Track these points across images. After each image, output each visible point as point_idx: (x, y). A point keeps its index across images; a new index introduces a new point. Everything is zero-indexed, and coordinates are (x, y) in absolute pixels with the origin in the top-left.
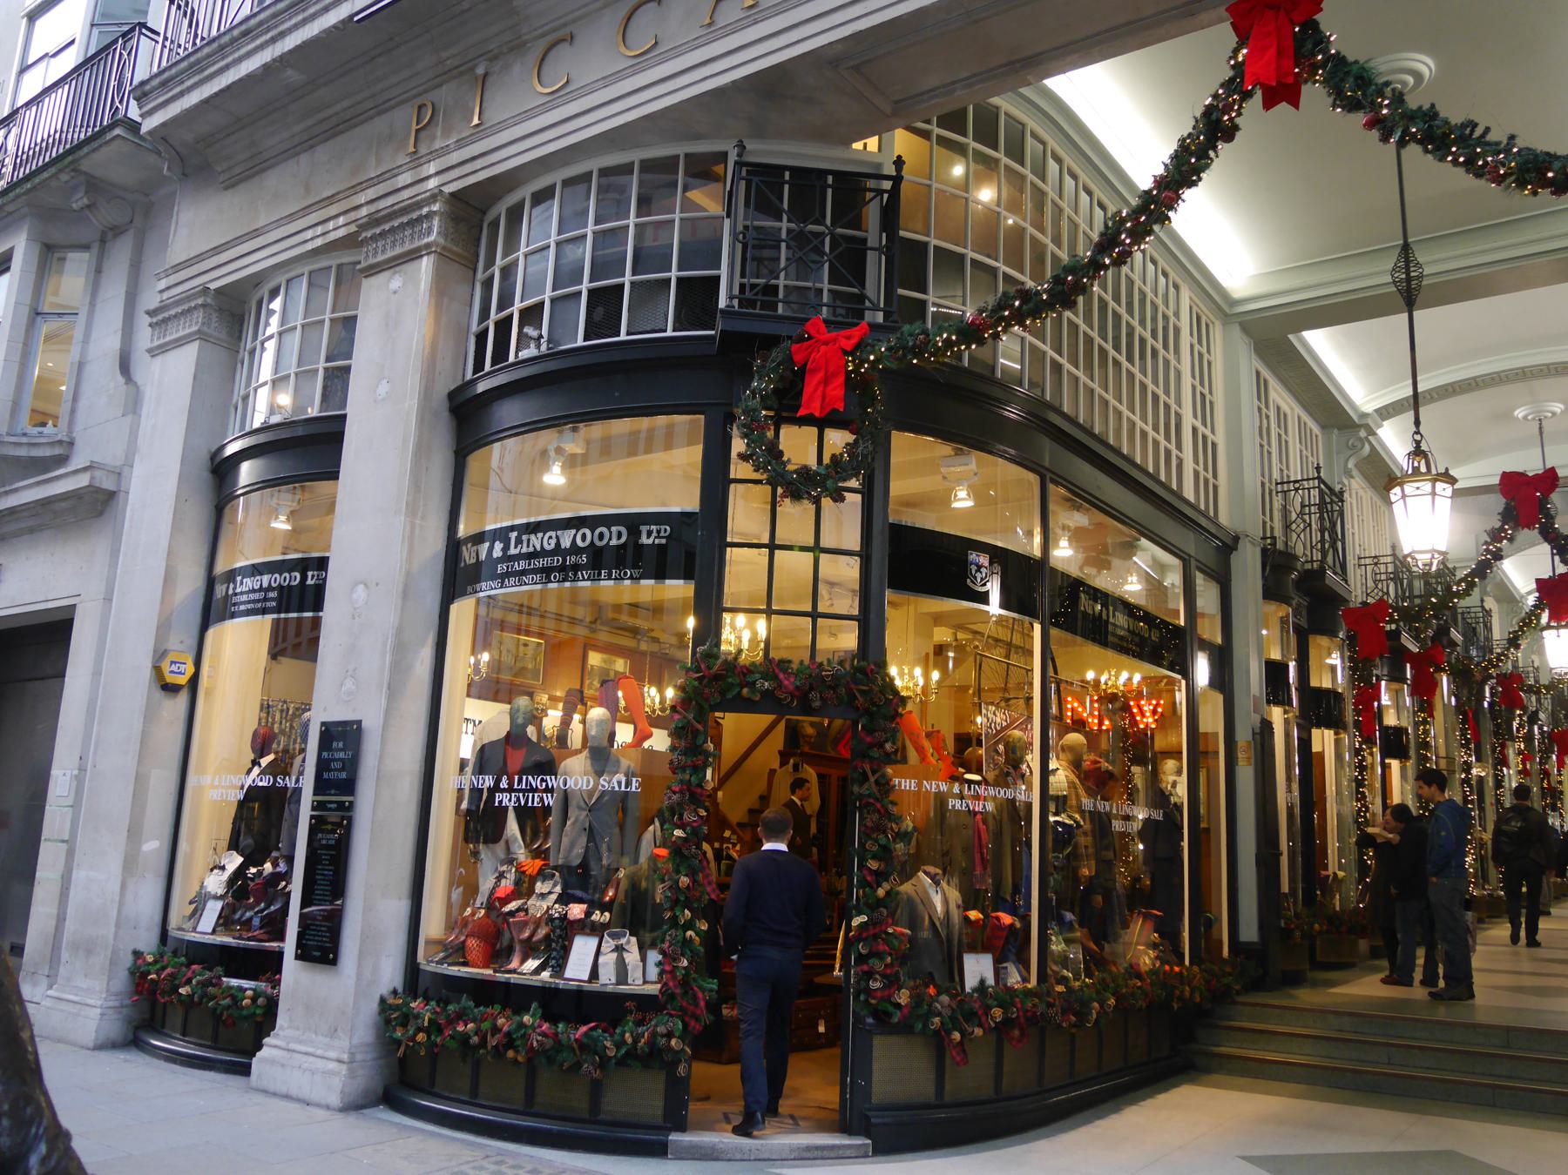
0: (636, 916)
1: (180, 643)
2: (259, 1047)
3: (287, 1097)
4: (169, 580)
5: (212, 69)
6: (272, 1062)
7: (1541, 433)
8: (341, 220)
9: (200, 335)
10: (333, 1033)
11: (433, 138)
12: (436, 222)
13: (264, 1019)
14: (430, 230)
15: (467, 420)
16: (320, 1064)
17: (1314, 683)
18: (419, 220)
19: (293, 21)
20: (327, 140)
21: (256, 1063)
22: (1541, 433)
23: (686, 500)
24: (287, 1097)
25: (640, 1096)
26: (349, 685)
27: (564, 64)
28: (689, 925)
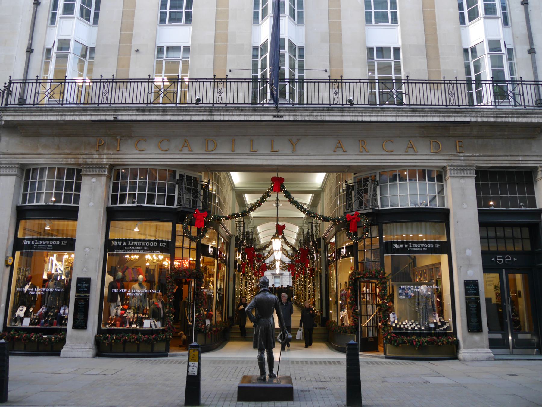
0: (155, 315)
1: (10, 253)
2: (62, 348)
3: (74, 357)
4: (8, 238)
5: (34, 114)
6: (64, 351)
7: (512, 375)
8: (73, 160)
9: (16, 175)
10: (86, 343)
11: (104, 149)
12: (107, 170)
13: (63, 342)
14: (105, 171)
15: (112, 215)
16: (84, 350)
17: (497, 275)
18: (102, 168)
19: (69, 114)
20: (59, 135)
21: (62, 352)
22: (512, 375)
23: (169, 238)
24: (74, 357)
25: (161, 347)
26: (85, 269)
27: (142, 145)
28: (172, 316)
